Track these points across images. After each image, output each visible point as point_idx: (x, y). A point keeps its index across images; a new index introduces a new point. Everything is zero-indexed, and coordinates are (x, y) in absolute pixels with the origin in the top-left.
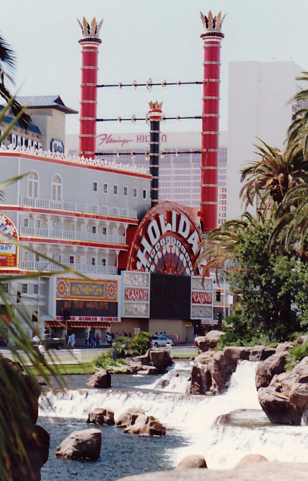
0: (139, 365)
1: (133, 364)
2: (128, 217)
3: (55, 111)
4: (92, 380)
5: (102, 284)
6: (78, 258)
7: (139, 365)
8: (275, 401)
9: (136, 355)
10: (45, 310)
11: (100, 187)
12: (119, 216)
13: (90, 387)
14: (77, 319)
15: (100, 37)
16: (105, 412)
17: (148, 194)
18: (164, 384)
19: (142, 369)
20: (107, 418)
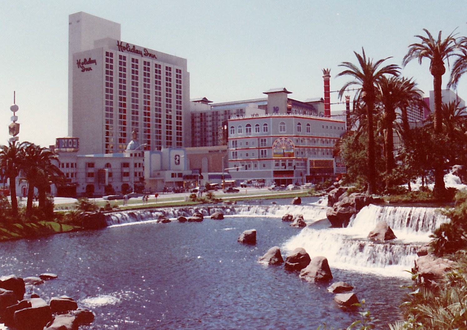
0: (325, 192)
1: (323, 192)
2: (336, 137)
3: (321, 103)
4: (293, 201)
5: (327, 162)
6: (317, 153)
7: (325, 192)
8: (333, 215)
9: (325, 189)
10: (306, 172)
11: (325, 127)
12: (333, 137)
13: (291, 204)
14: (318, 174)
15: (330, 75)
16: (289, 216)
17: (110, 134)
18: (320, 202)
19: (326, 194)
20: (290, 218)
